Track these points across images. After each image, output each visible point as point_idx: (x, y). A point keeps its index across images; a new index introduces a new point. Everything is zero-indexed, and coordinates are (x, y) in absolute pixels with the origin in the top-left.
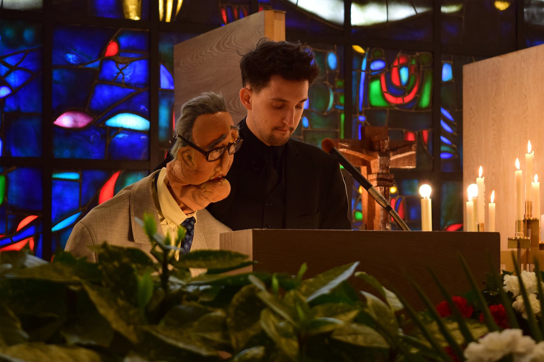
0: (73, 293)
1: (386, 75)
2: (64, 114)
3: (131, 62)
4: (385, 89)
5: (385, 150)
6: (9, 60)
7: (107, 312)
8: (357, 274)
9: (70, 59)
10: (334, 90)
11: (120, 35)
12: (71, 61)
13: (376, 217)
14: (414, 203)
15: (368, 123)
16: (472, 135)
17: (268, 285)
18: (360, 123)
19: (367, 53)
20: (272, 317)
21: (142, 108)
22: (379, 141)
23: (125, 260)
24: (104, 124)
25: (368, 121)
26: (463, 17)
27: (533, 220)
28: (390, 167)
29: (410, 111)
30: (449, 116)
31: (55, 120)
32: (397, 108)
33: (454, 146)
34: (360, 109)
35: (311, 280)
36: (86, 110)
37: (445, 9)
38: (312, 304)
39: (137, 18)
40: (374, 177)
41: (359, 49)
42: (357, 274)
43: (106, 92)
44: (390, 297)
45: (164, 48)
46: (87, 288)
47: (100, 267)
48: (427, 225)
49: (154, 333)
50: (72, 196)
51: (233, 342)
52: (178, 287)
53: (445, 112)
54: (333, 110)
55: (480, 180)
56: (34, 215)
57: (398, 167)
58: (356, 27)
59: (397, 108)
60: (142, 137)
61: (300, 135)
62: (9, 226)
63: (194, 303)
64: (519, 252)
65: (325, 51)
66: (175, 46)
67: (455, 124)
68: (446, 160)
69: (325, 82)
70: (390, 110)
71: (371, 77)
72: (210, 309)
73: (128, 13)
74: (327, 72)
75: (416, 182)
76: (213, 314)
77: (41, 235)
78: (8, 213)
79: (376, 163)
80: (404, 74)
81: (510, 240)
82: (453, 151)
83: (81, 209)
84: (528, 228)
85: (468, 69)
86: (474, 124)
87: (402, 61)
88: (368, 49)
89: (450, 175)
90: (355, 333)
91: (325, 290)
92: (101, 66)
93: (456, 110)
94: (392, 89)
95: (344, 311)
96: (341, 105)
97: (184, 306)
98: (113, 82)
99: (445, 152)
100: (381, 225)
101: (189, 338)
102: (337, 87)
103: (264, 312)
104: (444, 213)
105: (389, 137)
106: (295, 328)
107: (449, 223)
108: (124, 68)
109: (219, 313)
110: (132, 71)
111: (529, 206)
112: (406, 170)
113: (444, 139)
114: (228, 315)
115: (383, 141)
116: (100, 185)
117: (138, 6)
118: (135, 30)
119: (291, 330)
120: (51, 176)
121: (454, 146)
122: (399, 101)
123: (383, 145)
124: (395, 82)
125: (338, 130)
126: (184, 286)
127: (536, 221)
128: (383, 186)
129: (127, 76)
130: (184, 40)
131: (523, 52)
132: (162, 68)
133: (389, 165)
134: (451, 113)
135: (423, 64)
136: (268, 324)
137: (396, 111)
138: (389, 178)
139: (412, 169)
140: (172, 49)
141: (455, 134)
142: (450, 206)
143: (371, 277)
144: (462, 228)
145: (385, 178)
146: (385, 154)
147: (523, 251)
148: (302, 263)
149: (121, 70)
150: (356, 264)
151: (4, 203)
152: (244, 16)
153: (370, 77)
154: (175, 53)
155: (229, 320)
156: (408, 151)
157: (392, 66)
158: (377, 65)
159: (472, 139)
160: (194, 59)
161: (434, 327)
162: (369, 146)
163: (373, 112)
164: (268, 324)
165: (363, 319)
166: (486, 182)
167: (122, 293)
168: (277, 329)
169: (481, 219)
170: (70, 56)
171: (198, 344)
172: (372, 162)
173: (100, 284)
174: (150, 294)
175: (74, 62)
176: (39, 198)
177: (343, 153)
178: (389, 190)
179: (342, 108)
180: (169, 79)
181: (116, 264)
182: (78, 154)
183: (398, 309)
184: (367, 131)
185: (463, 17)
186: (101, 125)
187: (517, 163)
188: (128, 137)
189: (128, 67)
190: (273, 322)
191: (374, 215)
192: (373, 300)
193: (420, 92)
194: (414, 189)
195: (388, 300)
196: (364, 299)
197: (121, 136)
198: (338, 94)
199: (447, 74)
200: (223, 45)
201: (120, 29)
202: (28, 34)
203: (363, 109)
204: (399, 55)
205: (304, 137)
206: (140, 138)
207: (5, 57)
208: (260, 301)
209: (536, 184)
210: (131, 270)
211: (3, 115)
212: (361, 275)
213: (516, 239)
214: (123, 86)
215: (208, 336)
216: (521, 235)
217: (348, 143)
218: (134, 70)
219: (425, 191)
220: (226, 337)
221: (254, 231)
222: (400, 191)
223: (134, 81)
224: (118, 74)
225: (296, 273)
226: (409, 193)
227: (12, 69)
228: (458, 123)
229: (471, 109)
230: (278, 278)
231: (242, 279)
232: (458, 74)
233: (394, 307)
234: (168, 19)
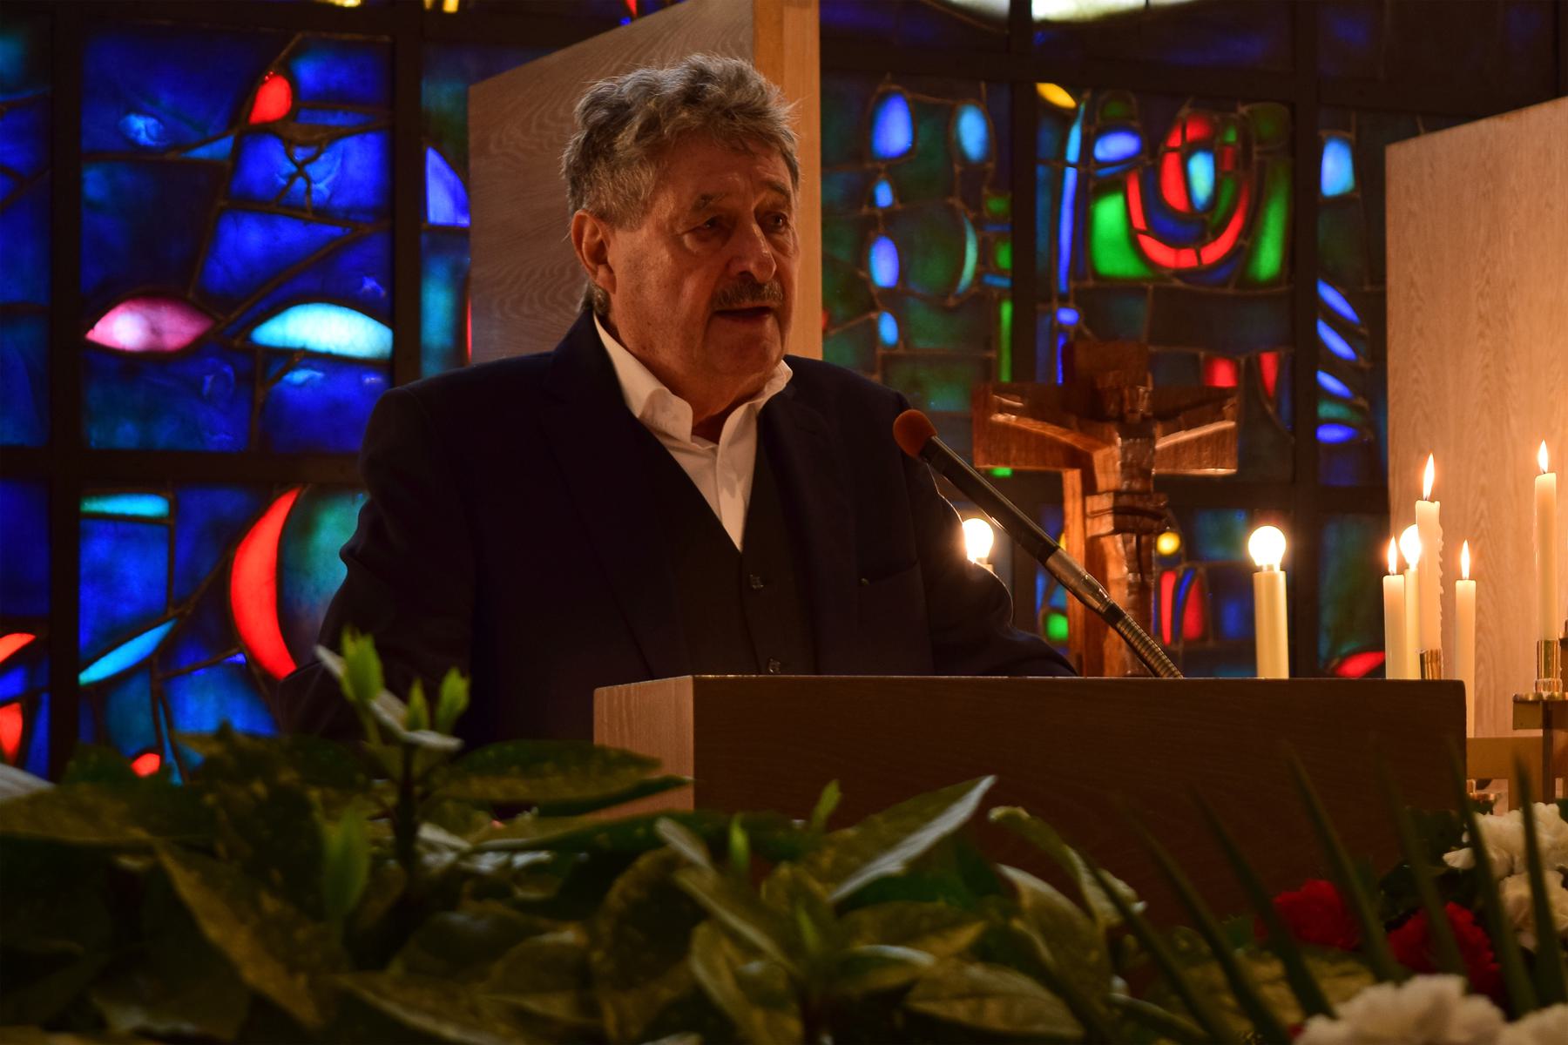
0: (129, 875)
1: (1144, 177)
2: (121, 308)
3: (335, 137)
4: (1139, 223)
5: (1138, 417)
7: (228, 934)
8: (996, 813)
9: (138, 132)
10: (978, 225)
11: (296, 53)
12: (143, 137)
15: (1087, 332)
16: (1415, 366)
17: (718, 848)
18: (1062, 329)
19: (1082, 107)
20: (727, 947)
21: (369, 285)
23: (287, 776)
24: (248, 338)
25: (1088, 323)
28: (1154, 472)
30: (1344, 308)
31: (92, 327)
32: (1178, 283)
33: (1362, 402)
34: (1063, 288)
35: (850, 833)
40: (1105, 502)
41: (1057, 95)
42: (996, 813)
43: (253, 237)
45: (438, 95)
46: (169, 862)
48: (1274, 661)
49: (370, 996)
50: (142, 572)
51: (610, 1022)
52: (449, 857)
53: (1330, 296)
54: (976, 290)
55: (1427, 509)
56: (21, 631)
58: (1046, 24)
59: (1178, 283)
60: (370, 380)
61: (873, 372)
63: (497, 908)
64: (1548, 741)
66: (473, 90)
67: (1363, 331)
68: (1333, 447)
69: (951, 201)
72: (542, 922)
74: (957, 168)
75: (1239, 518)
76: (549, 939)
77: (45, 697)
79: (1109, 461)
80: (1201, 172)
81: (1519, 702)
82: (1356, 418)
83: (171, 612)
85: (1402, 157)
86: (1420, 332)
87: (1193, 132)
88: (1087, 95)
89: (1346, 500)
90: (978, 993)
91: (891, 864)
92: (238, 154)
93: (1367, 288)
94: (1160, 219)
95: (942, 926)
96: (1001, 273)
98: (277, 204)
99: (1332, 422)
101: (474, 1011)
102: (986, 214)
103: (702, 932)
104: (1328, 617)
105: (1150, 377)
106: (791, 979)
109: (569, 935)
110: (336, 170)
113: (1328, 381)
115: (1133, 387)
116: (235, 534)
118: (346, 37)
119: (781, 985)
121: (1362, 402)
122: (1187, 259)
123: (1135, 400)
124: (1173, 197)
125: (992, 354)
126: (464, 855)
128: (1132, 532)
129: (321, 186)
132: (433, 159)
133: (1152, 464)
134: (1348, 298)
136: (712, 968)
138: (1151, 506)
141: (1363, 363)
142: (1340, 598)
144: (1381, 668)
145: (1140, 505)
146: (1138, 432)
148: (824, 782)
149: (301, 166)
150: (986, 783)
153: (1091, 185)
154: (472, 112)
155: (597, 956)
156: (1212, 422)
157: (1162, 148)
158: (1116, 146)
159: (1416, 381)
163: (1098, 294)
164: (712, 968)
165: (999, 949)
166: (1443, 517)
167: (276, 875)
168: (742, 981)
170: (139, 123)
171: (503, 1028)
172: (1098, 457)
173: (210, 852)
175: (150, 142)
178: (1153, 545)
179: (1005, 283)
180: (454, 195)
182: (164, 435)
184: (1081, 358)
186: (237, 343)
188: (322, 380)
189: (322, 157)
190: (729, 962)
192: (1034, 892)
194: (1235, 541)
196: (1011, 889)
197: (299, 376)
201: (299, 36)
203: (1072, 285)
204: (1185, 112)
205: (885, 377)
206: (361, 382)
210: (305, 808)
213: (1538, 700)
214: (309, 215)
215: (533, 1004)
217: (1022, 395)
218: (343, 165)
219: (1267, 547)
220: (590, 1008)
221: (698, 685)
223: (341, 202)
225: (806, 812)
226: (1217, 553)
229: (1412, 284)
230: (745, 826)
231: (640, 831)
232: (1369, 172)
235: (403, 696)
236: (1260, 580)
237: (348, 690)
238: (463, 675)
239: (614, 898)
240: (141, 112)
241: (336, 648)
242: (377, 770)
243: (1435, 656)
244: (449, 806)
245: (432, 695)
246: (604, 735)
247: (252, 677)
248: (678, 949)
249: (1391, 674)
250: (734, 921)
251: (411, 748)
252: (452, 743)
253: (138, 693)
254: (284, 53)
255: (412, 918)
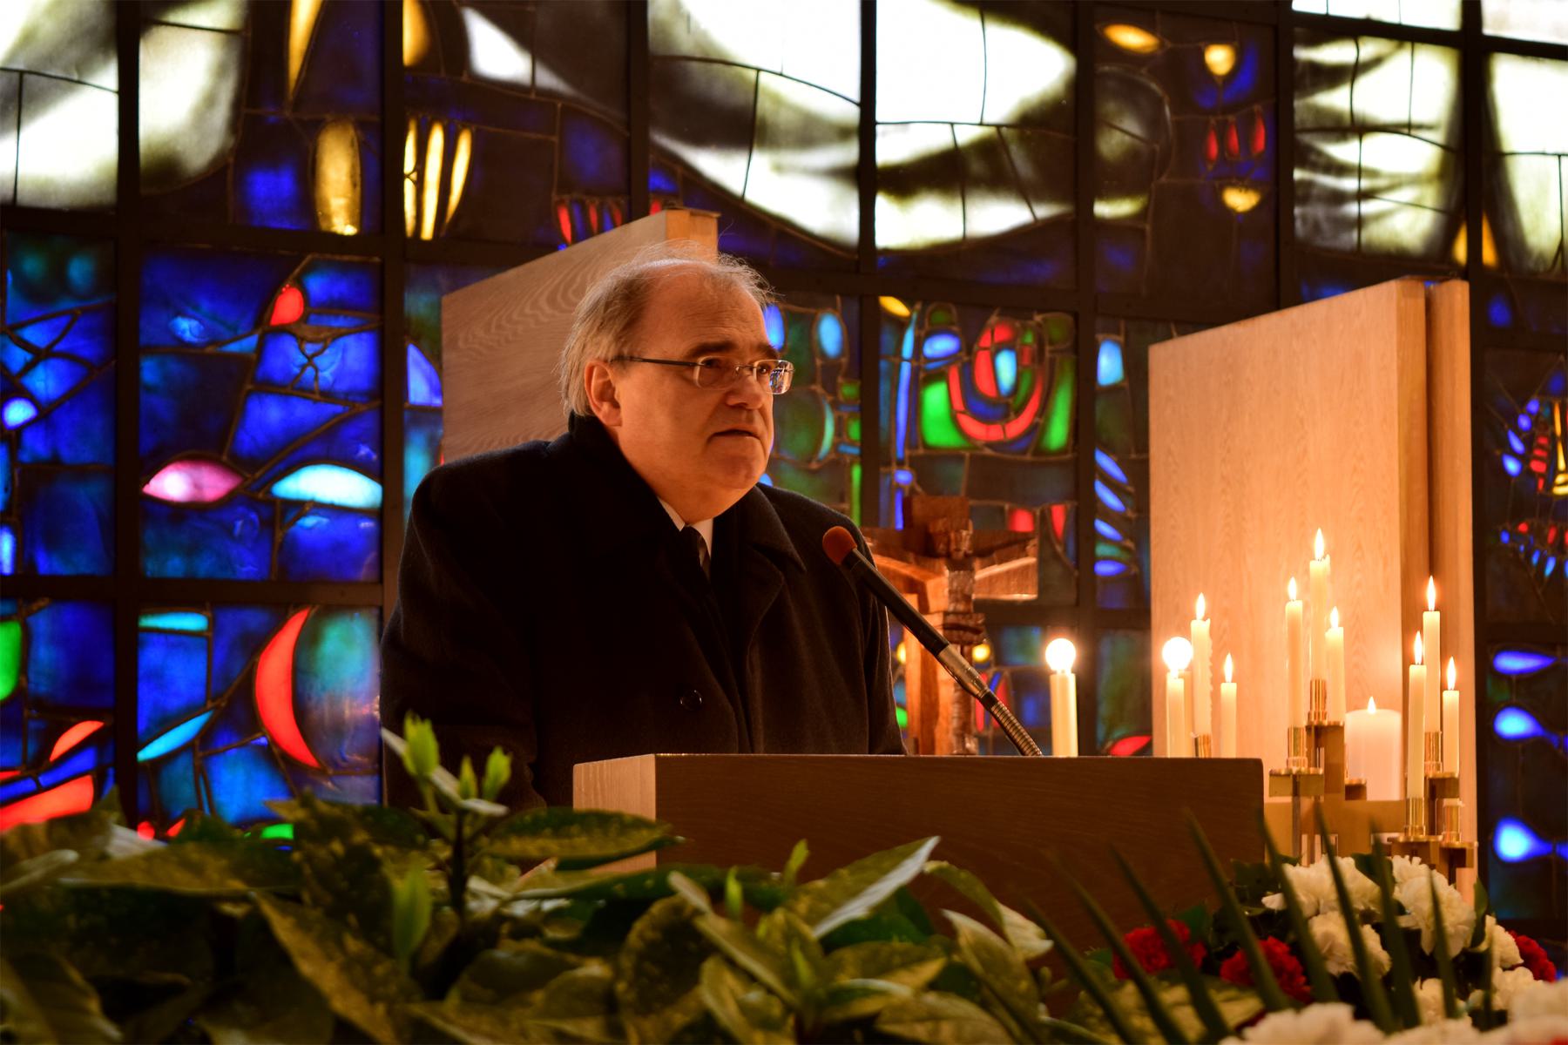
0: (230, 919)
1: (963, 371)
2: (170, 468)
3: (337, 336)
4: (959, 405)
5: (961, 554)
6: (33, 335)
7: (318, 969)
10: (835, 406)
11: (308, 270)
13: (941, 720)
14: (1031, 687)
15: (919, 489)
17: (717, 895)
18: (900, 488)
19: (915, 316)
20: (730, 980)
22: (947, 533)
23: (360, 837)
24: (269, 492)
26: (1148, 228)
27: (1329, 726)
28: (974, 597)
29: (1019, 458)
31: (148, 482)
33: (1129, 544)
34: (900, 454)
35: (820, 884)
36: (225, 458)
37: (1105, 209)
38: (830, 943)
39: (350, 230)
41: (895, 306)
44: (1012, 924)
45: (417, 304)
46: (269, 910)
47: (297, 856)
49: (438, 1022)
50: (187, 674)
52: (490, 905)
53: (1105, 461)
54: (833, 456)
57: (994, 596)
59: (988, 452)
62: (32, 748)
63: (532, 945)
64: (1296, 806)
65: (812, 311)
66: (445, 299)
67: (1130, 489)
68: (1108, 579)
69: (813, 387)
70: (971, 457)
71: (926, 374)
72: (571, 958)
73: (328, 217)
75: (1035, 634)
77: (111, 771)
78: (27, 717)
80: (1006, 367)
83: (210, 705)
84: (1317, 745)
88: (918, 306)
89: (1119, 613)
90: (934, 1017)
91: (857, 909)
92: (261, 349)
93: (1133, 456)
94: (976, 402)
95: (910, 962)
96: (852, 443)
97: (505, 952)
98: (293, 388)
99: (1107, 559)
100: (953, 740)
102: (841, 398)
103: (710, 967)
104: (1104, 710)
106: (788, 1009)
107: (1117, 734)
108: (317, 354)
109: (595, 969)
110: (340, 360)
111: (1319, 692)
112: (1012, 604)
113: (1103, 528)
114: (618, 974)
115: (957, 531)
116: (257, 644)
117: (353, 201)
118: (346, 258)
119: (776, 1010)
120: (136, 621)
121: (1129, 544)
122: (995, 433)
123: (959, 541)
124: (984, 385)
126: (505, 903)
127: (1337, 729)
130: (466, 284)
131: (1294, 314)
132: (413, 354)
133: (972, 591)
134: (1120, 463)
135: (1051, 343)
136: (720, 994)
137: (985, 458)
138: (971, 623)
139: (1027, 603)
140: (438, 307)
141: (1130, 514)
142: (1118, 696)
143: (964, 875)
144: (1148, 747)
145: (963, 622)
146: (961, 565)
147: (1306, 803)
150: (931, 843)
151: (18, 696)
152: (614, 226)
153: (922, 375)
154: (446, 316)
155: (621, 987)
157: (976, 348)
158: (941, 346)
160: (493, 330)
161: (1128, 996)
162: (923, 545)
163: (928, 461)
164: (720, 994)
165: (955, 981)
167: (352, 919)
168: (744, 1008)
169: (1204, 726)
172: (931, 585)
173: (297, 899)
174: (424, 923)
175: (195, 340)
176: (97, 678)
177: (886, 571)
179: (855, 451)
180: (429, 381)
181: (337, 847)
182: (204, 567)
183: (1032, 955)
184: (917, 508)
185: (1148, 228)
186: (260, 495)
187: (1293, 587)
190: (732, 992)
191: (937, 715)
192: (974, 933)
193: (1045, 410)
194: (1034, 652)
195: (1008, 930)
196: (950, 931)
197: (309, 521)
198: (845, 416)
199: (1109, 366)
200: (564, 296)
201: (309, 257)
202: (79, 270)
203: (907, 452)
204: (993, 319)
207: (23, 325)
208: (698, 936)
209: (1335, 634)
210: (375, 863)
211: (16, 473)
212: (940, 870)
214: (317, 397)
215: (570, 1027)
216: (1301, 765)
218: (343, 359)
219: (1061, 656)
221: (657, 759)
222: (998, 656)
223: (342, 386)
224: (303, 367)
225: (780, 865)
226: (1019, 660)
227: (39, 356)
228: (1138, 487)
230: (739, 878)
231: (649, 883)
232: (1136, 367)
233: (1022, 948)
234: (427, 232)
235: (455, 771)
236: (1055, 683)
237: (410, 765)
238: (505, 753)
239: (633, 938)
240: (185, 315)
241: (400, 732)
242: (432, 831)
243: (1207, 739)
244: (487, 862)
245: (480, 770)
246: (583, 800)
247: (275, 759)
248: (693, 979)
249: (1157, 753)
250: (744, 959)
251: (463, 813)
252: (499, 810)
253: (183, 767)
254: (297, 271)
255: (463, 958)
